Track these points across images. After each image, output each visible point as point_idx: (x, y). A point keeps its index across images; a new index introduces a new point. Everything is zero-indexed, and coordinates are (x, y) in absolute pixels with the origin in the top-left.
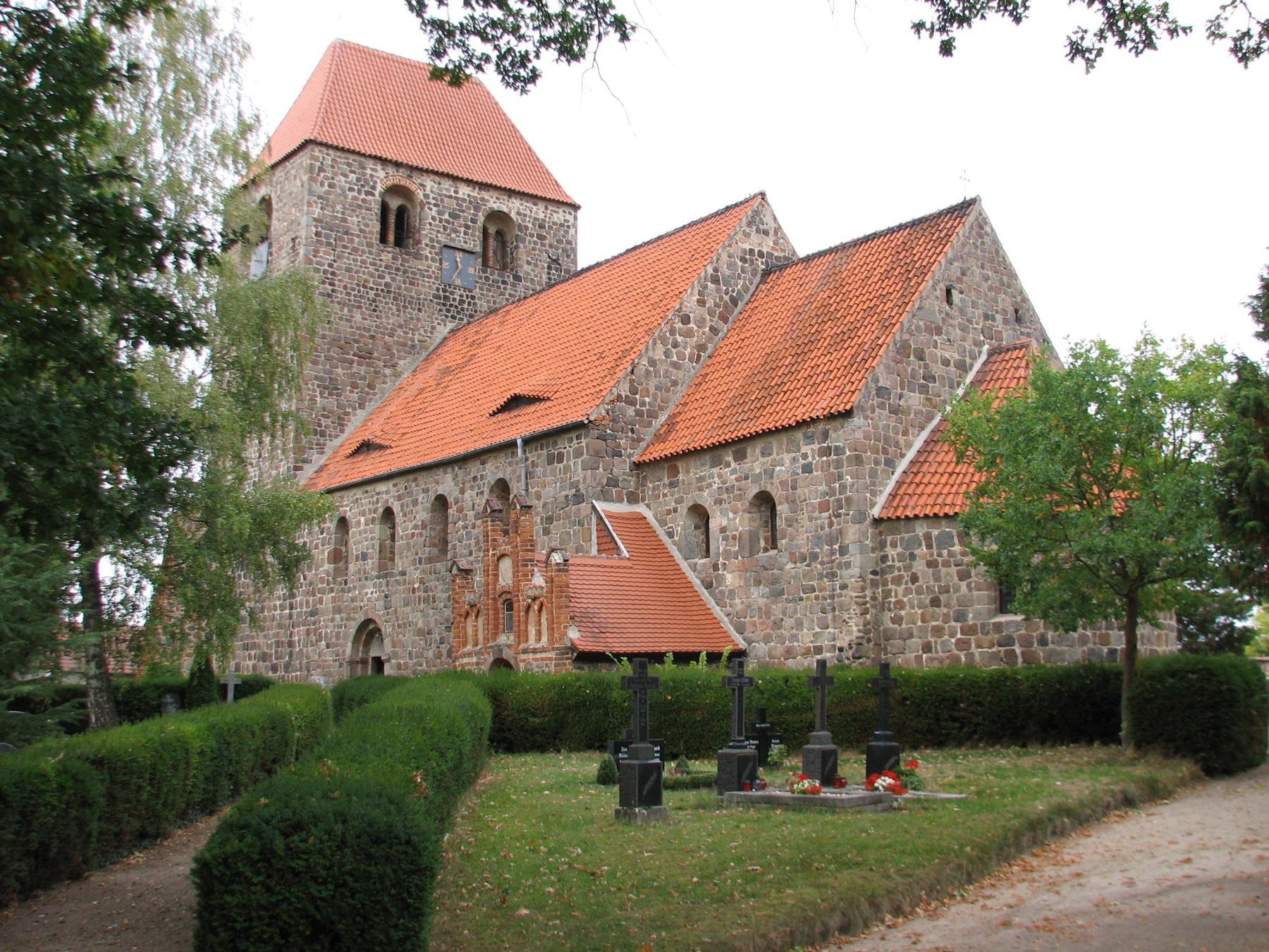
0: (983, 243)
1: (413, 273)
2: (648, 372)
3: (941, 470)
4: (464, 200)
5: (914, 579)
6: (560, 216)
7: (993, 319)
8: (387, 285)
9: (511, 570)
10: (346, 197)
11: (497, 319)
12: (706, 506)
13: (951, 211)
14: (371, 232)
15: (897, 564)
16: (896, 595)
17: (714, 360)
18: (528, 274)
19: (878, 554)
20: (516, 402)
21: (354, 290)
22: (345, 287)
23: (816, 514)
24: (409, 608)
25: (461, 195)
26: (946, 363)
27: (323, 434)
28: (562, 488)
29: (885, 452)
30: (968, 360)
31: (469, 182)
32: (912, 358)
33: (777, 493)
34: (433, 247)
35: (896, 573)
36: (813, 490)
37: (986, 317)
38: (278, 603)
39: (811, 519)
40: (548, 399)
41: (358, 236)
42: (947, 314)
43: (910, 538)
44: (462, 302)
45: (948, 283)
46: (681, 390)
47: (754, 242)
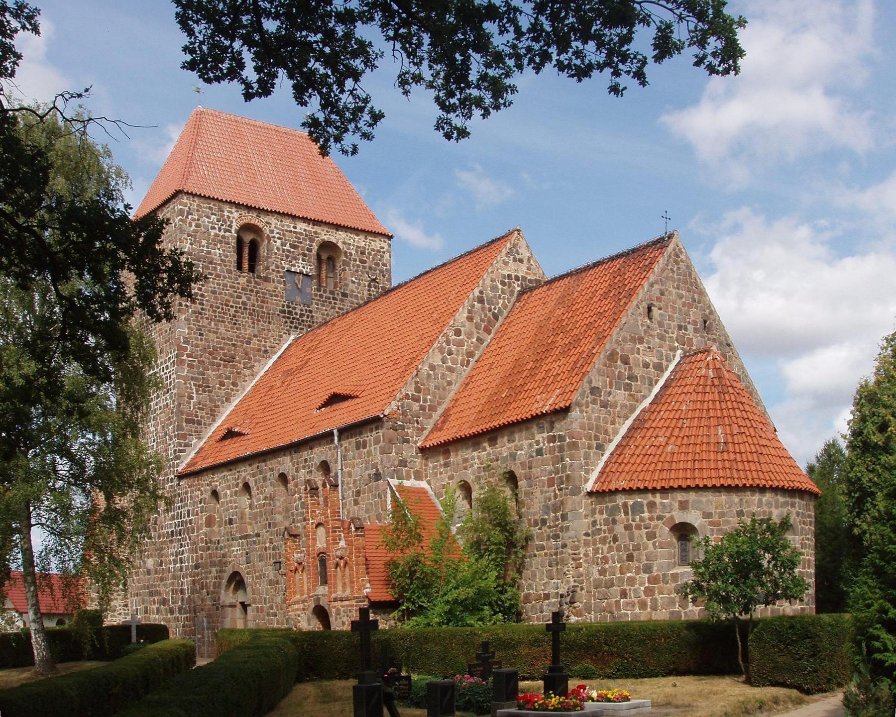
0: (679, 268)
1: (263, 293)
2: (429, 375)
3: (637, 452)
4: (301, 234)
5: (615, 539)
6: (378, 244)
7: (686, 329)
8: (244, 303)
9: (324, 535)
10: (209, 234)
11: (327, 329)
12: (470, 481)
13: (654, 243)
14: (229, 261)
15: (604, 528)
16: (602, 553)
17: (479, 364)
18: (353, 291)
19: (590, 520)
20: (335, 399)
21: (218, 308)
22: (212, 306)
23: (546, 488)
24: (263, 563)
25: (298, 230)
26: (646, 365)
27: (199, 423)
28: (367, 468)
29: (597, 438)
30: (664, 363)
31: (305, 220)
32: (619, 363)
33: (519, 472)
34: (278, 272)
35: (603, 535)
36: (543, 470)
37: (680, 328)
38: (172, 558)
39: (542, 492)
40: (357, 397)
41: (220, 265)
42: (648, 327)
43: (613, 507)
44: (302, 315)
45: (649, 302)
46: (455, 388)
47: (511, 269)
